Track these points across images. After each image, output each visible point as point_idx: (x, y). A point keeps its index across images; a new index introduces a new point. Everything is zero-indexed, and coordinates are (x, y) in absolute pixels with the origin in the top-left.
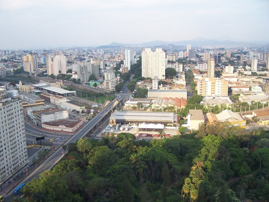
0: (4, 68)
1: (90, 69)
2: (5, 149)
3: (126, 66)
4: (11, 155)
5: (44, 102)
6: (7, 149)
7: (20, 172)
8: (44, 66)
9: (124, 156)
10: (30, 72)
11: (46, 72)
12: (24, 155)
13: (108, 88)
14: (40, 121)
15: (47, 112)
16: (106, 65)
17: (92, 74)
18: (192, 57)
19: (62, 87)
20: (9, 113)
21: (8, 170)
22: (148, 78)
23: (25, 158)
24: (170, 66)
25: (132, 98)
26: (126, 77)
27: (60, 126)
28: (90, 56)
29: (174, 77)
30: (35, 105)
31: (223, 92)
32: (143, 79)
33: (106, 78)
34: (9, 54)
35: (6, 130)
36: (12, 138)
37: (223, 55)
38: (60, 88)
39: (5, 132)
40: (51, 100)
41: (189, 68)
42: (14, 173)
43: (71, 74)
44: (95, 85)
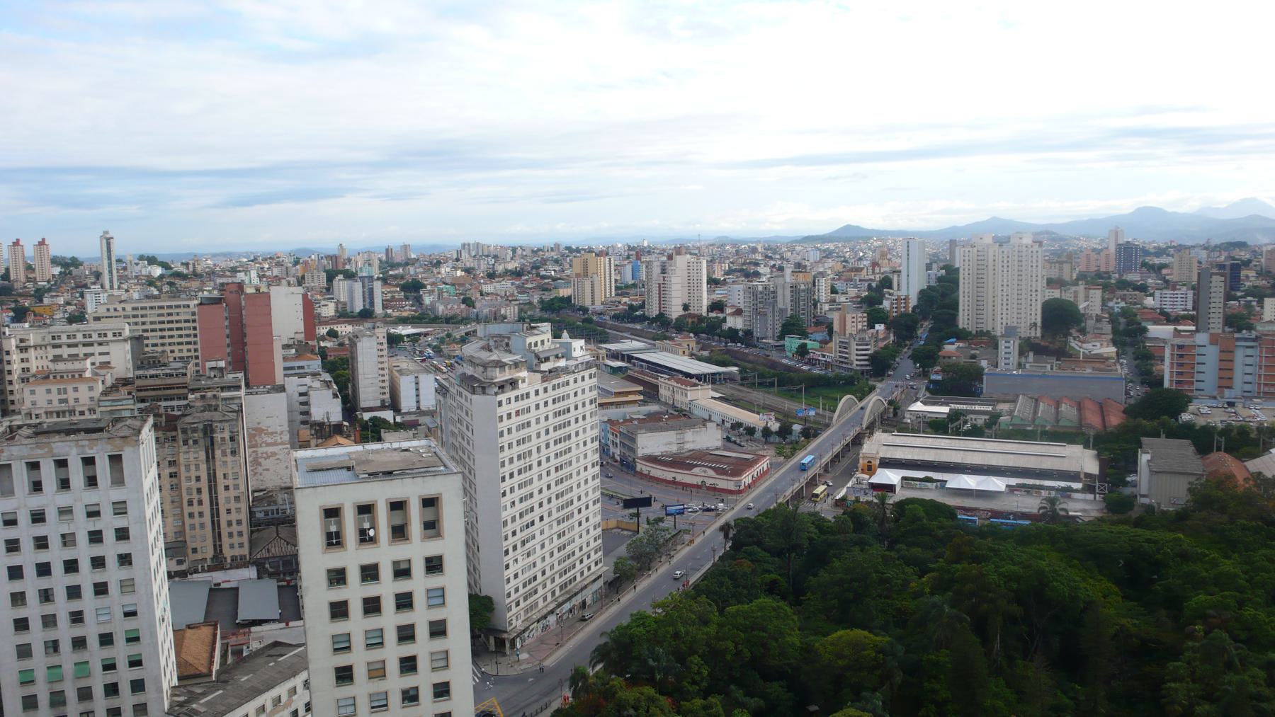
0: (512, 295)
1: (784, 301)
2: (542, 519)
3: (903, 293)
4: (556, 542)
5: (640, 393)
6: (546, 519)
7: (577, 601)
8: (632, 291)
9: (933, 570)
10: (591, 308)
11: (643, 306)
12: (593, 545)
13: (845, 361)
14: (633, 450)
15: (653, 422)
16: (834, 291)
17: (792, 317)
18: (1129, 269)
19: (692, 355)
20: (557, 405)
21: (545, 587)
22: (980, 333)
23: (593, 557)
24: (1056, 294)
25: (928, 395)
26: (903, 326)
27: (696, 470)
28: (774, 266)
29: (1073, 331)
30: (612, 404)
31: (1266, 385)
32: (961, 335)
33: (836, 327)
34: (523, 257)
35: (548, 459)
36: (562, 487)
37: (1247, 263)
38: (686, 358)
39: (544, 465)
40: (662, 391)
41: (1123, 304)
42: (561, 600)
43: (721, 316)
44: (802, 351)
